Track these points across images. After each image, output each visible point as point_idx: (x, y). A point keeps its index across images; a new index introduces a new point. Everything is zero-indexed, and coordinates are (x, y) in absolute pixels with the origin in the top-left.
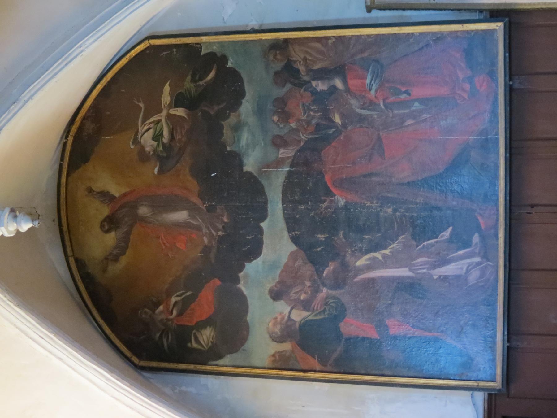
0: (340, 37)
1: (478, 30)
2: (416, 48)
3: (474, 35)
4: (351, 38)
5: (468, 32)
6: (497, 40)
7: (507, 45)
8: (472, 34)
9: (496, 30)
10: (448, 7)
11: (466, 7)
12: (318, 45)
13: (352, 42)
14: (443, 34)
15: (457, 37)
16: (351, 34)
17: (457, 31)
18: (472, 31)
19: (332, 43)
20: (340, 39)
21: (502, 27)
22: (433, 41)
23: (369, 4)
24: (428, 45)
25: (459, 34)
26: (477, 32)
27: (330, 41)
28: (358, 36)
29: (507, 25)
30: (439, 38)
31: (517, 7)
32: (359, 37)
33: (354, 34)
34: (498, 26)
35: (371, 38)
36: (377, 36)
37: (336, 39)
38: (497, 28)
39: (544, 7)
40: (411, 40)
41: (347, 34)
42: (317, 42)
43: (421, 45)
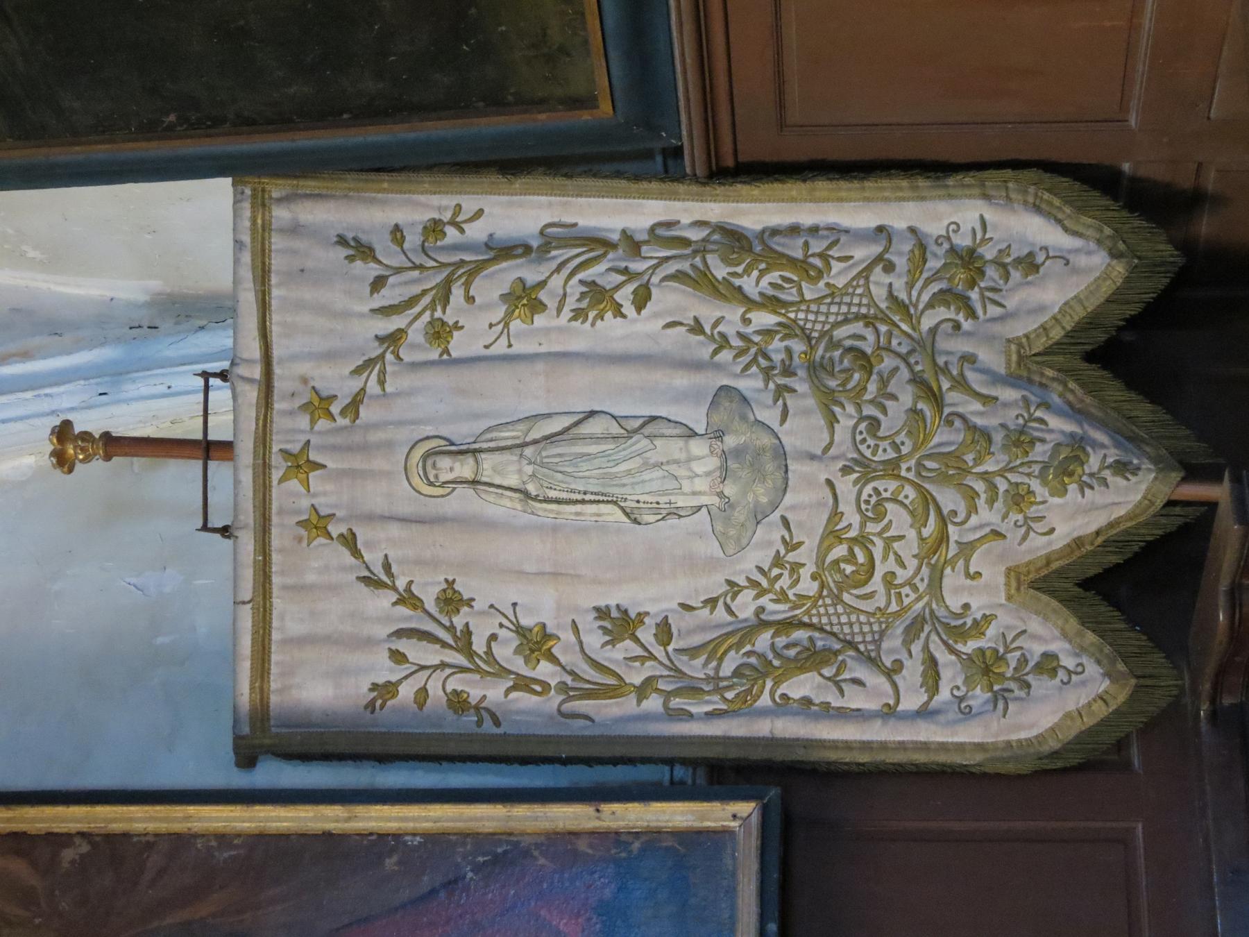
0: (110, 838)
1: (658, 832)
2: (405, 895)
3: (643, 850)
4: (150, 843)
5: (615, 838)
6: (734, 874)
7: (774, 889)
8: (636, 845)
9: (726, 833)
10: (550, 751)
11: (618, 751)
12: (18, 867)
13: (155, 861)
14: (516, 844)
15: (576, 854)
16: (151, 827)
17: (575, 834)
18: (637, 835)
19: (73, 862)
20: (113, 846)
21: (755, 820)
22: (477, 869)
23: (246, 730)
24: (452, 884)
25: (582, 845)
26: (652, 837)
27: (68, 855)
28: (178, 836)
29: (776, 818)
30: (503, 854)
31: (815, 756)
32: (180, 841)
33: (163, 827)
34: (734, 815)
35: (231, 846)
36: (261, 839)
37: (94, 845)
38: (734, 824)
39: (921, 758)
40: (390, 863)
41: (139, 827)
42: (18, 853)
43: (426, 882)
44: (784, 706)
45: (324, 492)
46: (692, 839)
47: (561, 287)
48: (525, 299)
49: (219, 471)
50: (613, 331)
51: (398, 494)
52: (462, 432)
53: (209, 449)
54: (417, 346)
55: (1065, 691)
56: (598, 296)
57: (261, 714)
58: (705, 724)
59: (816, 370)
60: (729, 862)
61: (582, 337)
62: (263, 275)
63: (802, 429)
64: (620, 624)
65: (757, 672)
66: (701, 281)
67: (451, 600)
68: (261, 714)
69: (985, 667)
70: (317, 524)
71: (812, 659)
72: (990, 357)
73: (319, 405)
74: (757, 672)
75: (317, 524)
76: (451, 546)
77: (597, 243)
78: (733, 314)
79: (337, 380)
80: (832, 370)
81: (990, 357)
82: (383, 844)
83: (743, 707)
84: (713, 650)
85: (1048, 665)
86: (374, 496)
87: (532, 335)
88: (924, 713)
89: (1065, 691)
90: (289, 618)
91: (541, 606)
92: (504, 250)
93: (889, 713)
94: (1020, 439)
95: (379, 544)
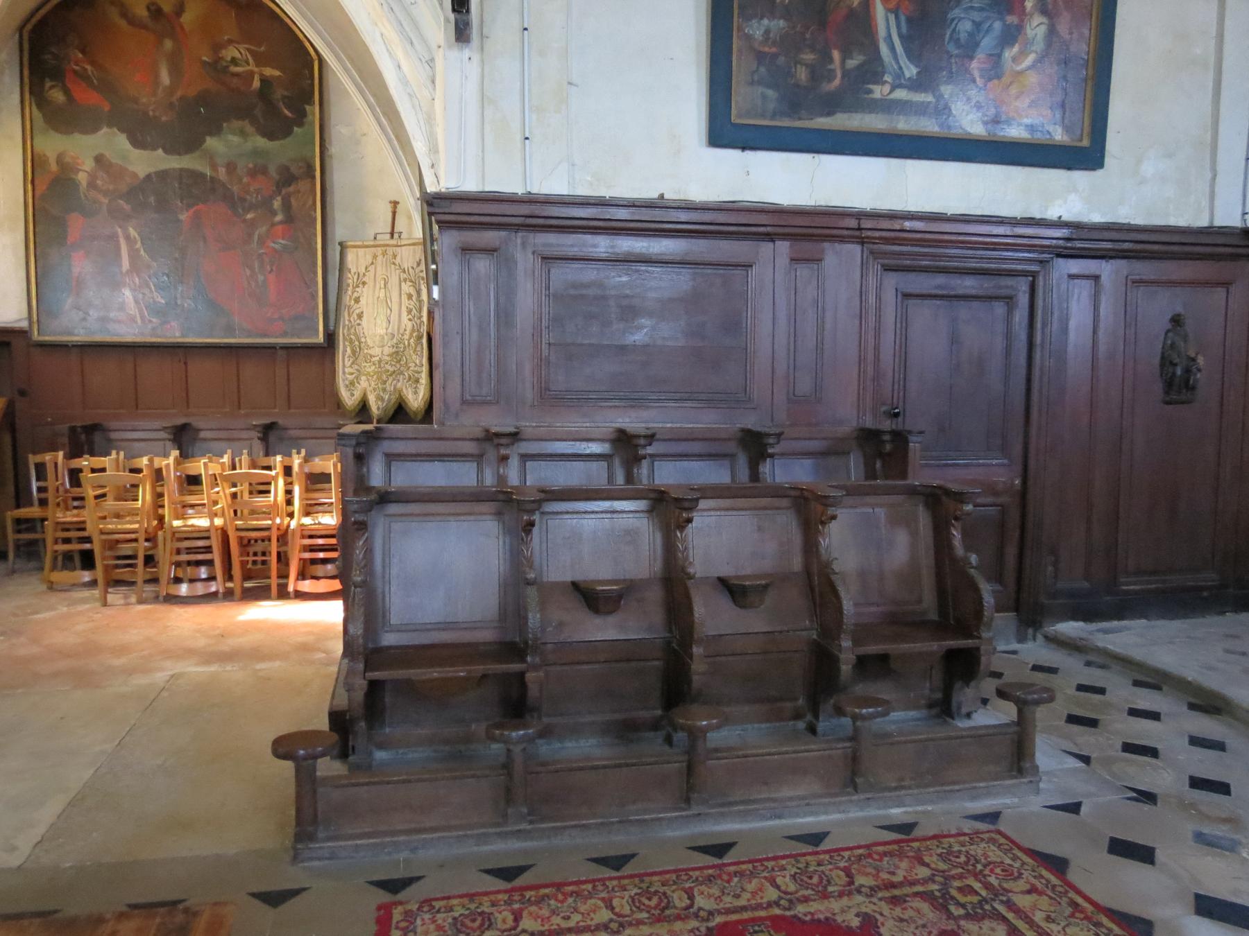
32: (315, 235)
34: (321, 338)
44: (345, 347)
45: (380, 258)
46: (317, 330)
47: (412, 304)
48: (410, 297)
49: (388, 236)
50: (404, 314)
51: (379, 272)
52: (389, 285)
53: (392, 234)
54: (404, 276)
55: (350, 399)
56: (409, 312)
57: (347, 247)
58: (341, 333)
59: (397, 353)
60: (545, 310)
61: (404, 309)
62: (414, 244)
63: (387, 350)
64: (360, 316)
65: (351, 342)
66: (413, 330)
67: (364, 283)
68: (347, 247)
69: (352, 383)
70: (375, 257)
71: (354, 352)
72: (399, 385)
73: (395, 256)
74: (351, 342)
75: (375, 257)
76: (371, 283)
77: (420, 310)
78: (406, 337)
79: (398, 261)
80: (397, 355)
81: (399, 385)
82: (315, 273)
83: (345, 339)
84: (355, 334)
85: (352, 395)
86: (379, 268)
87: (404, 297)
88: (344, 373)
89: (350, 399)
90: (361, 251)
91: (363, 301)
92: (419, 292)
93: (344, 366)
94: (384, 390)
95: (372, 268)
